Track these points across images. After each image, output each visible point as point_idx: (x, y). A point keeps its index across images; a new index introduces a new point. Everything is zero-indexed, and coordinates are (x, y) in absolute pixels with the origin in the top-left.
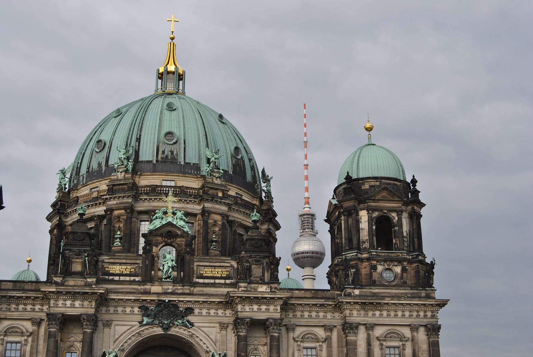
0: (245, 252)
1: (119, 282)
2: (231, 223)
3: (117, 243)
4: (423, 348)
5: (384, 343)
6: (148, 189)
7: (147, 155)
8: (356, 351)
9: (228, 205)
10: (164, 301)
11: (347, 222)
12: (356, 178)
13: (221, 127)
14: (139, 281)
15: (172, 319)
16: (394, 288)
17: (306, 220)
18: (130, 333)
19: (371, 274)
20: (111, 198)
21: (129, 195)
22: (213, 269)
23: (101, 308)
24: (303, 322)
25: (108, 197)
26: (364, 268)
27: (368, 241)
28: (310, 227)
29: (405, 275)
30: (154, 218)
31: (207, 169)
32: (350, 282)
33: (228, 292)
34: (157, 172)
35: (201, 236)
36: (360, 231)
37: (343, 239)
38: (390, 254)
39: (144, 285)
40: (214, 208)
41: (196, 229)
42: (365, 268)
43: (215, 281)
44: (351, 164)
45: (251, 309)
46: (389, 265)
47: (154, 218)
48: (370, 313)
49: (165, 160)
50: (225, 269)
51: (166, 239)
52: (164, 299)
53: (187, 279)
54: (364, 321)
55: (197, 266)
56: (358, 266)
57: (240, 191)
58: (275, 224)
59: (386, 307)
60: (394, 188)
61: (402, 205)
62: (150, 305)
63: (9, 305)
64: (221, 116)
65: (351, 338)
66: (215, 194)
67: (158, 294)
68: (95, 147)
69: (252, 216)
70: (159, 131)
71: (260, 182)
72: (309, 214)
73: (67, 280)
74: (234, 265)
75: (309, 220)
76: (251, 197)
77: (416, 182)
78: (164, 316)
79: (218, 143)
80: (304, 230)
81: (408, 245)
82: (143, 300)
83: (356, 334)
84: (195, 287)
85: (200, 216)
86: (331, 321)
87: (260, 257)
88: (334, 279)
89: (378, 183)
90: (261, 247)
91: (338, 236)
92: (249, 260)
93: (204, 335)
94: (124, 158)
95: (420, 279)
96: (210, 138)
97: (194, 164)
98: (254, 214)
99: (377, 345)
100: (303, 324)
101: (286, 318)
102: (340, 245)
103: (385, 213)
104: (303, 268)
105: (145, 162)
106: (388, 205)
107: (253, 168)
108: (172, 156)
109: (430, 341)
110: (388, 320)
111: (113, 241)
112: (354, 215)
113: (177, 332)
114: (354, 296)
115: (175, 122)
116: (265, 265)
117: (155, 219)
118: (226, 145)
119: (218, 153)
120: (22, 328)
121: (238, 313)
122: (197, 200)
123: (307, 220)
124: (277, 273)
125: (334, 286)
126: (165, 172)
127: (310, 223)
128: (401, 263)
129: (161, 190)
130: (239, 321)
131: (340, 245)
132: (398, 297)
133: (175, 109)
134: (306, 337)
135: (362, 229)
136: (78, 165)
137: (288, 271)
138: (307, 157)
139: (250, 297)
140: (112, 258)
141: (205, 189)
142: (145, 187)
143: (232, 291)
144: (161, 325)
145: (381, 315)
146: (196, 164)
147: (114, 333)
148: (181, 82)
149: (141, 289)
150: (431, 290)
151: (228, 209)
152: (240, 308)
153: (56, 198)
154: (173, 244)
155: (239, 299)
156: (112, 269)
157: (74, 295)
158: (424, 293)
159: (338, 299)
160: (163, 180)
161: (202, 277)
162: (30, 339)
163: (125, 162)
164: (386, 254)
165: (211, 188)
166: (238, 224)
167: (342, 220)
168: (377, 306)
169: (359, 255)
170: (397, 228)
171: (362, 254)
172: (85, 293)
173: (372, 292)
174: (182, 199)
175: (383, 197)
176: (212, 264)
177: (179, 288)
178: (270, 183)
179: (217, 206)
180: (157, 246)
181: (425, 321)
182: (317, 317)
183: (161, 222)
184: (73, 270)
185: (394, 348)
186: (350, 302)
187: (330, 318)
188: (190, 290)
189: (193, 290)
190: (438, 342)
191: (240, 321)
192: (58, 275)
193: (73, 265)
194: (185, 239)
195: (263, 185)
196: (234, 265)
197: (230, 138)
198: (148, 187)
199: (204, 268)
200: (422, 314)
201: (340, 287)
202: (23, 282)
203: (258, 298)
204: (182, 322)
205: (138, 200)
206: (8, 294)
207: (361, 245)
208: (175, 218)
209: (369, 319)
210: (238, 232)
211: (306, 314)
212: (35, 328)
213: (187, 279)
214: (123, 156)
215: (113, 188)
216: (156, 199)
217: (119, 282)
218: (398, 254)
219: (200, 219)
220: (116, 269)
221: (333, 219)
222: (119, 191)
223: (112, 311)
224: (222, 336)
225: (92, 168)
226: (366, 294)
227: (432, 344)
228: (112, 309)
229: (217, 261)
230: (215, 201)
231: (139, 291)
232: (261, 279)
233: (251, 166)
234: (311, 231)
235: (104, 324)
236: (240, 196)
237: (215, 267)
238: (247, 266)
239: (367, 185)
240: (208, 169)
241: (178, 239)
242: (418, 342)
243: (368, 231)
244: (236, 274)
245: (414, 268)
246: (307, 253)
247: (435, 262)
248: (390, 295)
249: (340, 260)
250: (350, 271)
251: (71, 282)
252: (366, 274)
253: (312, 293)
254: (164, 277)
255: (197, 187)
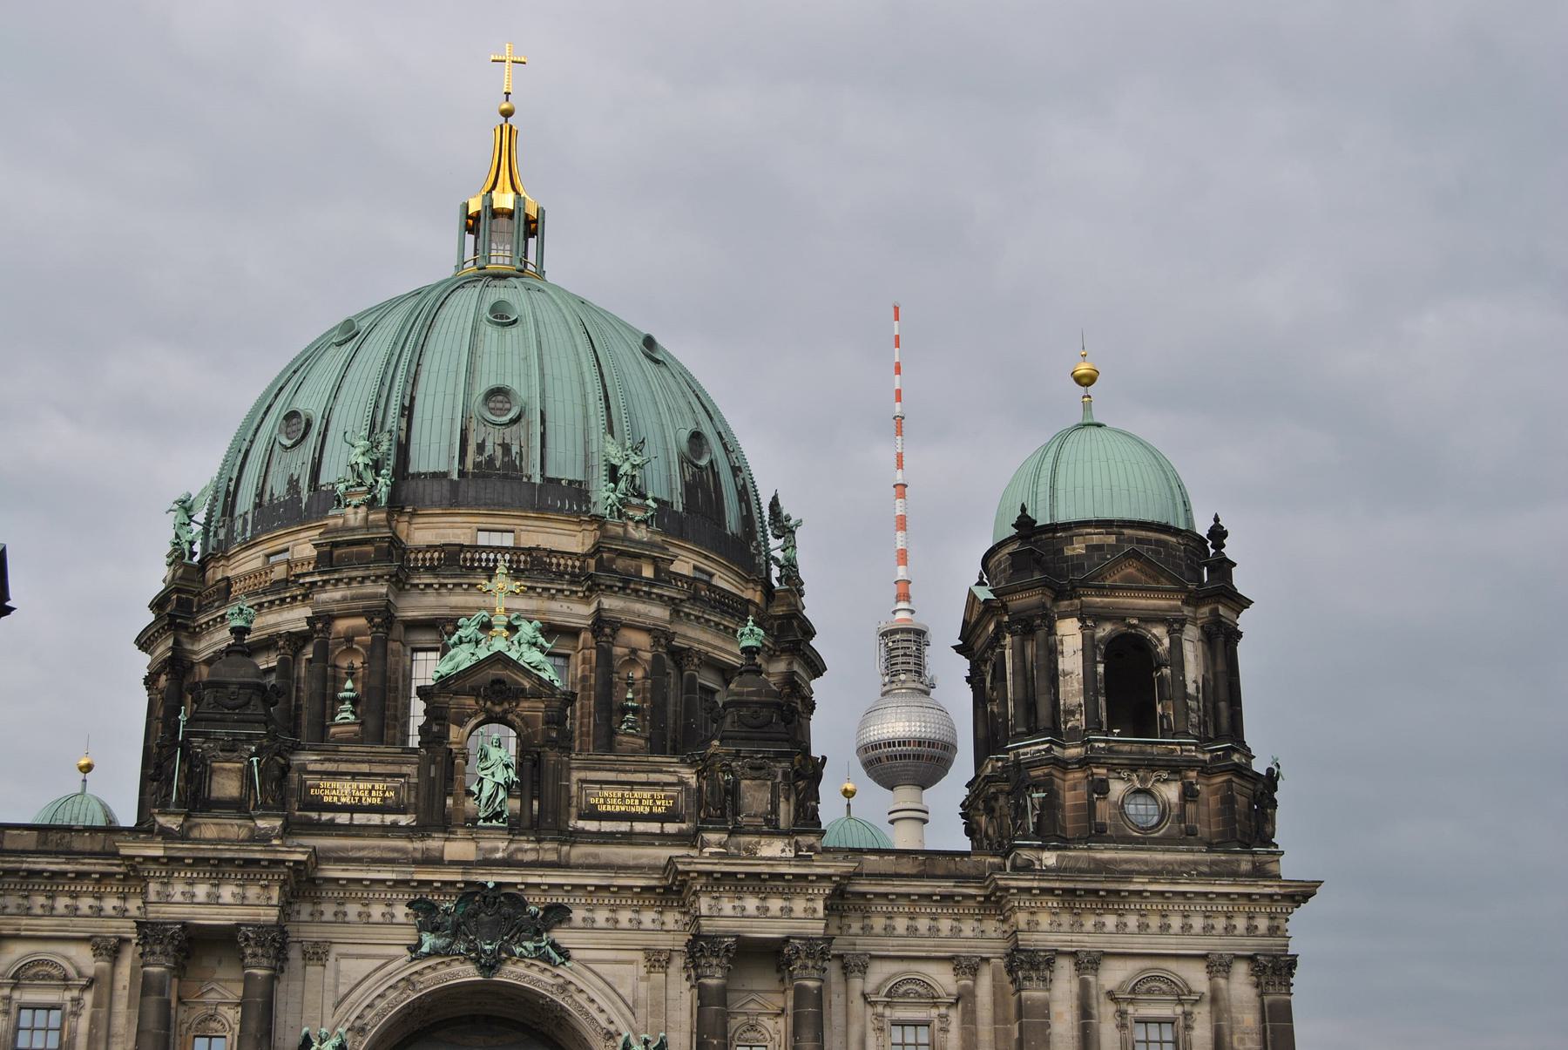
0: (721, 741)
1: (350, 830)
2: (680, 656)
3: (345, 714)
4: (1245, 1025)
5: (1130, 1009)
6: (436, 555)
7: (434, 455)
8: (1048, 1031)
9: (671, 602)
10: (484, 885)
11: (1020, 653)
12: (1048, 522)
13: (649, 372)
14: (408, 826)
15: (505, 938)
16: (1159, 847)
17: (900, 646)
18: (382, 981)
19: (1091, 806)
20: (325, 582)
21: (379, 572)
22: (627, 792)
23: (296, 907)
24: (890, 948)
25: (317, 578)
26: (1072, 788)
27: (1083, 709)
28: (912, 667)
29: (1190, 808)
30: (452, 641)
31: (609, 497)
32: (1029, 829)
33: (670, 858)
34: (463, 506)
35: (592, 693)
36: (1058, 678)
37: (1010, 704)
38: (1148, 748)
39: (422, 838)
40: (630, 612)
41: (576, 675)
42: (1074, 788)
43: (632, 826)
44: (1034, 483)
45: (738, 910)
46: (1143, 780)
47: (452, 641)
48: (1089, 922)
49: (485, 471)
50: (663, 791)
51: (489, 704)
52: (482, 879)
53: (550, 820)
54: (1070, 944)
55: (580, 784)
56: (1052, 782)
57: (705, 562)
58: (809, 660)
59: (1135, 904)
60: (1160, 553)
61: (1184, 602)
62: (442, 898)
63: (26, 897)
64: (649, 342)
65: (1033, 993)
66: (632, 570)
67: (465, 864)
68: (280, 432)
69: (742, 635)
70: (469, 384)
71: (765, 536)
72: (908, 631)
73: (198, 825)
74: (688, 778)
75: (909, 648)
76: (737, 579)
77: (1225, 534)
78: (484, 931)
79: (641, 421)
80: (895, 675)
81: (1202, 721)
82: (422, 883)
83: (1047, 982)
84: (573, 844)
85: (589, 635)
86: (973, 943)
87: (766, 755)
88: (983, 820)
89: (1112, 539)
90: (767, 725)
91: (995, 694)
92: (733, 764)
93: (601, 985)
94: (366, 465)
95: (1236, 821)
96: (619, 407)
97: (570, 482)
98: (747, 628)
99: (1110, 1015)
100: (892, 954)
101: (841, 935)
102: (1000, 720)
103: (1134, 626)
104: (892, 789)
105: (426, 477)
106: (1142, 602)
107: (745, 494)
108: (506, 459)
109: (1266, 1002)
110: (1140, 940)
111: (333, 708)
112: (1041, 633)
113: (520, 977)
114: (1042, 870)
115: (516, 358)
116: (779, 779)
117: (455, 645)
118: (665, 427)
119: (640, 451)
120: (66, 965)
121: (701, 922)
122: (581, 589)
123: (902, 648)
124: (814, 803)
125: (982, 842)
126: (486, 505)
127: (911, 656)
128: (1179, 772)
129: (472, 560)
130: (702, 943)
131: (1000, 720)
132: (1172, 873)
133: (515, 321)
134: (901, 990)
135: (1065, 674)
136: (228, 486)
137: (849, 798)
138: (904, 463)
139: (735, 874)
140: (329, 760)
141: (602, 556)
142: (427, 551)
143: (682, 857)
144: (473, 955)
145: (1121, 927)
146: (577, 481)
147: (337, 980)
148: (532, 242)
149: (415, 849)
150: (1269, 853)
151: (671, 614)
152: (706, 905)
153: (164, 581)
154: (510, 717)
155: (703, 880)
156: (331, 790)
157: (216, 868)
158: (1248, 861)
159: (995, 879)
160: (479, 530)
161: (593, 814)
162: (88, 998)
163: (369, 477)
164: (1135, 748)
165: (621, 554)
166: (700, 659)
167: (1007, 647)
168: (1110, 900)
169: (1057, 751)
170: (1167, 671)
171: (1064, 747)
172: (249, 862)
173: (1095, 860)
174: (535, 585)
175: (1127, 578)
176: (623, 777)
177: (527, 848)
178: (794, 538)
179: (639, 607)
180: (461, 724)
181: (1250, 945)
182: (934, 931)
183: (473, 654)
184: (214, 794)
185: (1160, 1023)
186: (1029, 890)
187: (971, 934)
188: (558, 852)
189: (568, 854)
190: (1288, 1006)
191: (706, 943)
192: (172, 809)
193: (215, 778)
194: (543, 702)
195: (774, 543)
196: (690, 780)
197: (675, 406)
198: (436, 551)
199: (601, 789)
200: (1240, 923)
201: (1001, 845)
202: (69, 829)
203: (758, 875)
204: (535, 947)
205: (407, 587)
206: (25, 866)
207: (1062, 719)
208: (516, 642)
209: (1086, 939)
210: (700, 683)
211: (901, 924)
212: (104, 964)
213: (550, 820)
214: (361, 460)
215: (331, 553)
216: (460, 585)
217: (350, 830)
218: (1170, 747)
219: (589, 645)
220: (343, 791)
221: (979, 643)
222: (349, 562)
223: (328, 916)
224: (653, 988)
225: (272, 495)
226: (1078, 866)
227: (1270, 1011)
228: (329, 910)
229: (640, 768)
230: (633, 590)
231: (409, 856)
232: (768, 822)
233: (740, 488)
234: (916, 678)
235: (305, 953)
236: (705, 577)
237: (632, 784)
238: (727, 782)
239: (1079, 543)
240: (613, 496)
241: (525, 704)
242: (1230, 1006)
243: (1082, 680)
244: (694, 806)
245: (1219, 789)
246: (904, 745)
247: (1281, 770)
248: (1146, 869)
249: (1000, 764)
250: (1030, 796)
251: (209, 829)
252: (1076, 804)
253: (917, 863)
254: (482, 815)
255: (579, 550)
